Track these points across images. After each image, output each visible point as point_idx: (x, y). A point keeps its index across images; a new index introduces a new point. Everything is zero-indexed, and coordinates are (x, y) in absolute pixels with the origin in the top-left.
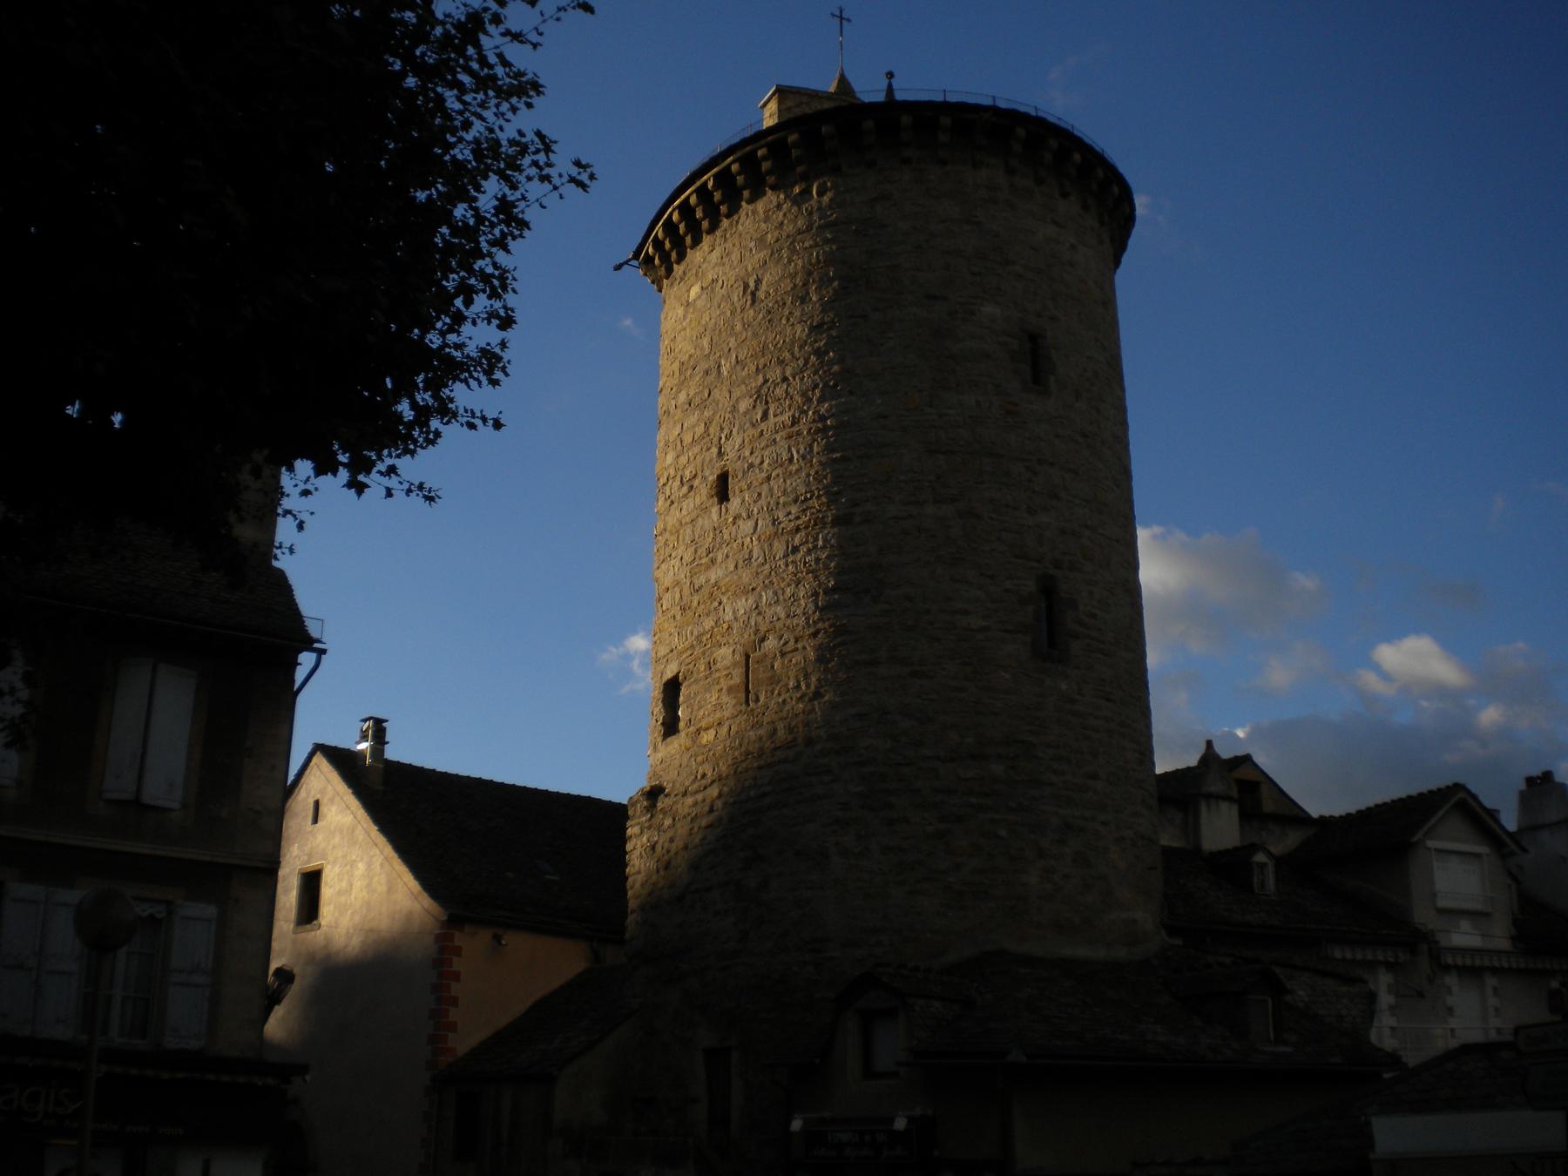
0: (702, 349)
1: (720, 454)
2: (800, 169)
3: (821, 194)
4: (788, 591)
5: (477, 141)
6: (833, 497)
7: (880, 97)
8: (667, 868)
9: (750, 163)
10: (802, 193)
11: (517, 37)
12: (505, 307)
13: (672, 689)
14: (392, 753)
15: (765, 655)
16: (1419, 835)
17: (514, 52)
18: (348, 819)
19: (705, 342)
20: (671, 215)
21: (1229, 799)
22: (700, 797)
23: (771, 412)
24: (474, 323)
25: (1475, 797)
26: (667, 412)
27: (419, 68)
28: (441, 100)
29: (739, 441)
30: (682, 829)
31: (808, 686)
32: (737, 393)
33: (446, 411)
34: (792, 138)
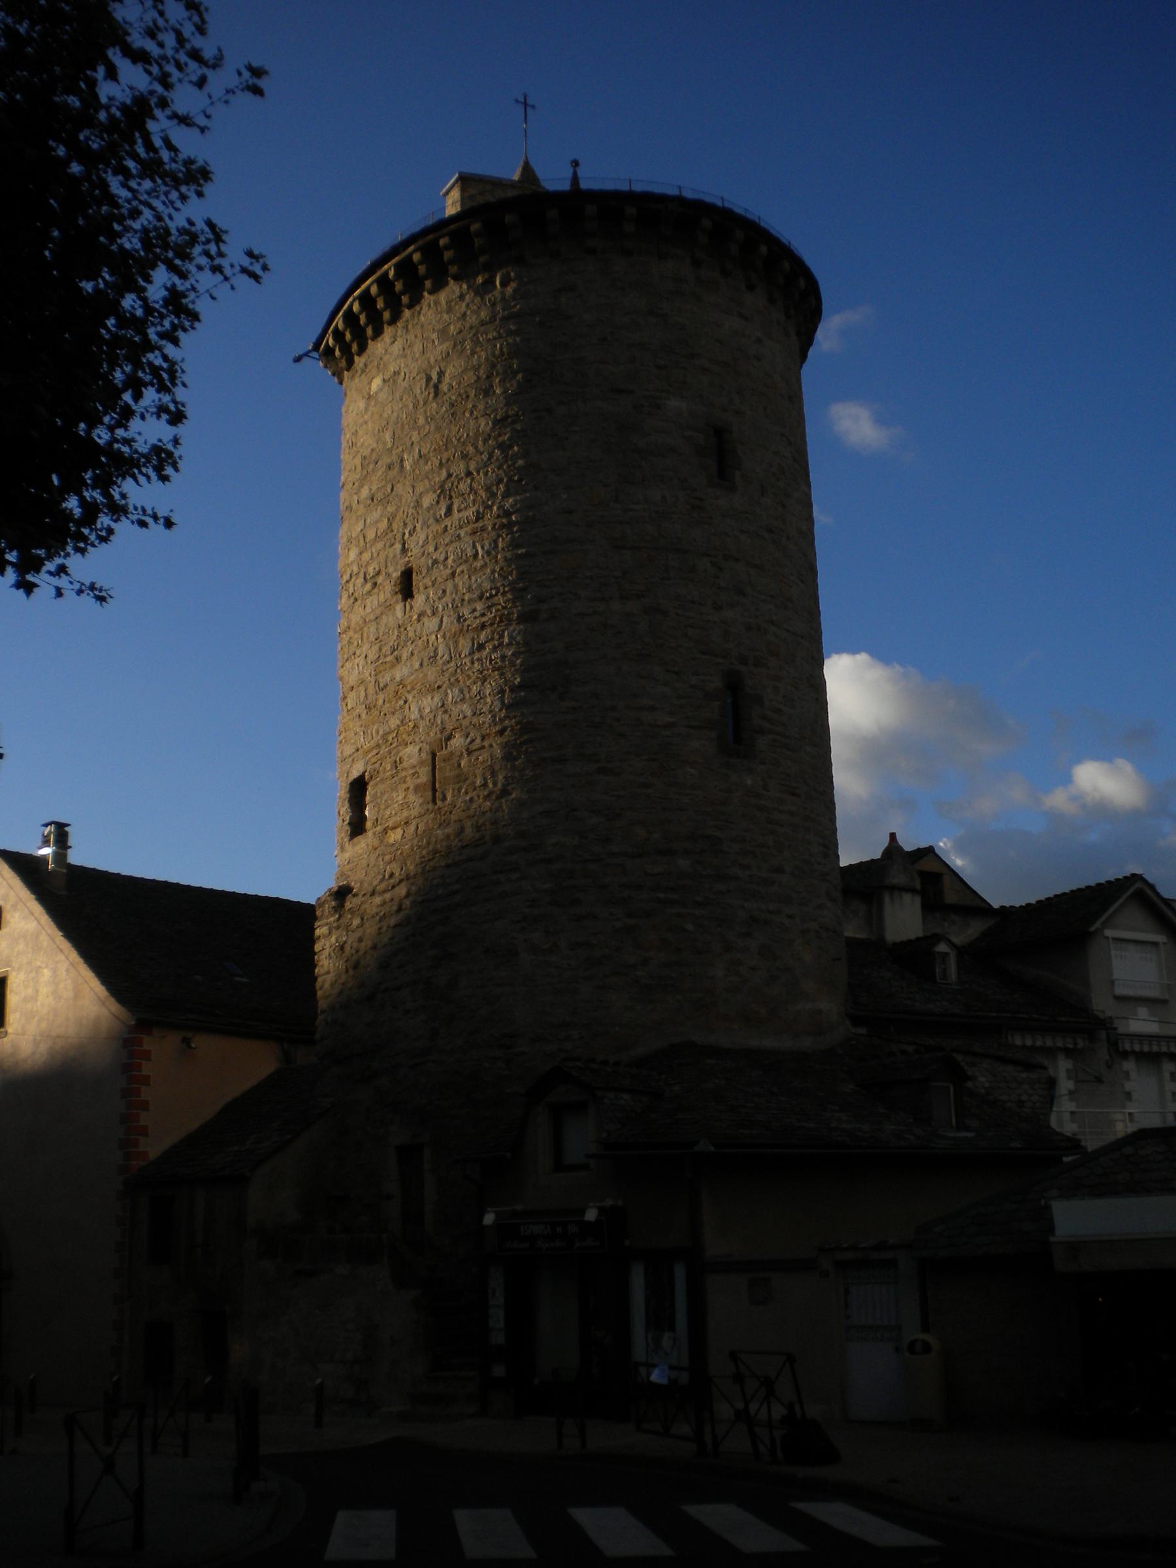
0: (385, 443)
1: (404, 550)
2: (483, 259)
3: (504, 284)
4: (474, 688)
5: (145, 231)
6: (518, 593)
7: (565, 186)
8: (356, 966)
9: (431, 252)
10: (485, 283)
11: (184, 120)
12: (175, 402)
13: (358, 788)
14: (76, 857)
15: (452, 754)
16: (1097, 925)
17: (182, 137)
18: (32, 926)
19: (388, 436)
20: (351, 307)
21: (912, 890)
22: (388, 896)
23: (455, 507)
24: (143, 417)
25: (1152, 887)
26: (349, 508)
27: (80, 152)
28: (105, 186)
29: (423, 537)
30: (371, 929)
31: (495, 784)
32: (420, 488)
33: (118, 510)
34: (475, 227)
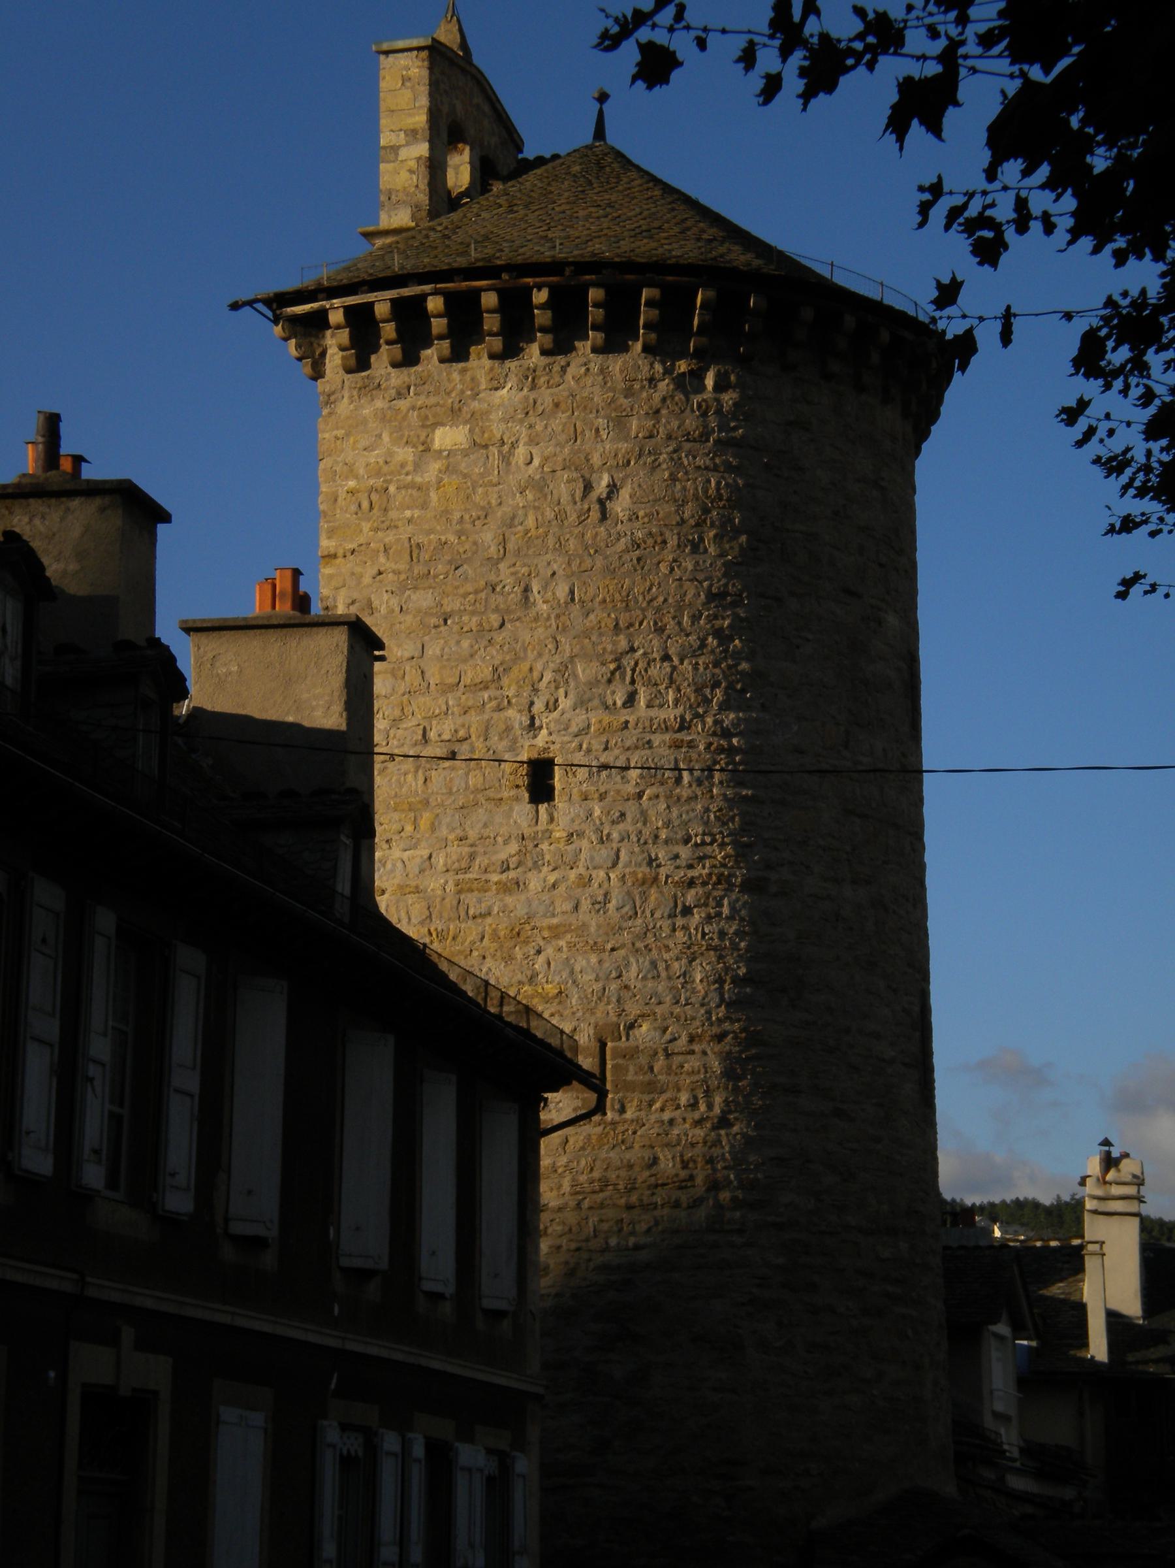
3: (720, 387)
6: (742, 852)
31: (710, 1106)
